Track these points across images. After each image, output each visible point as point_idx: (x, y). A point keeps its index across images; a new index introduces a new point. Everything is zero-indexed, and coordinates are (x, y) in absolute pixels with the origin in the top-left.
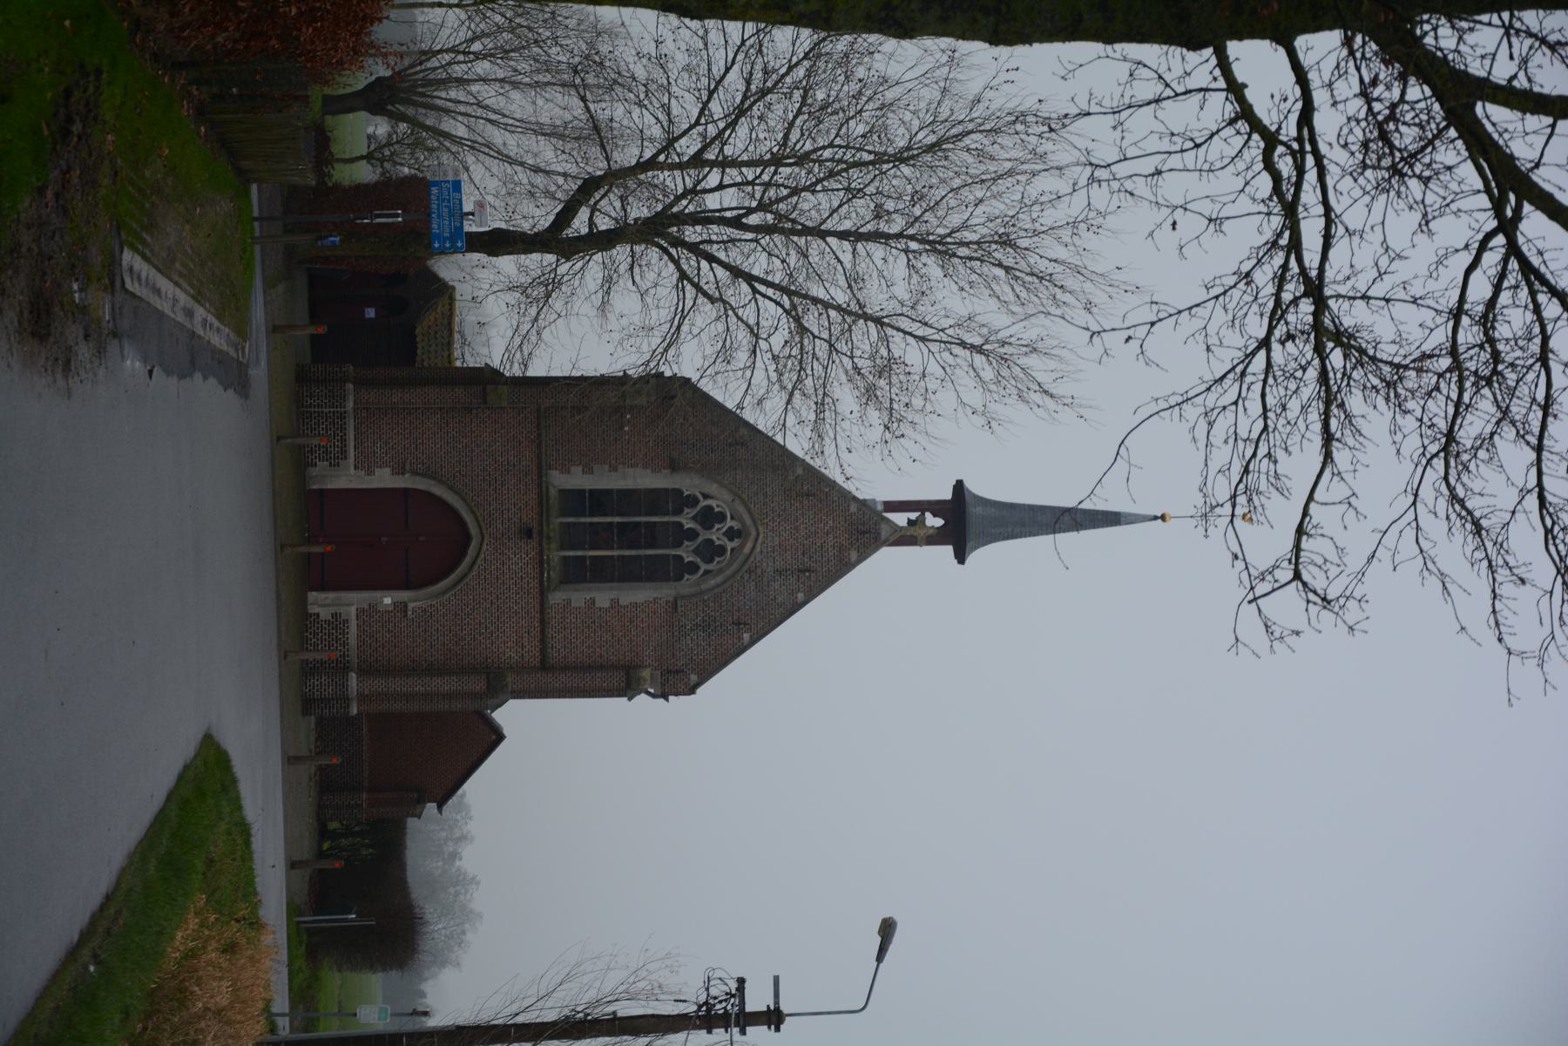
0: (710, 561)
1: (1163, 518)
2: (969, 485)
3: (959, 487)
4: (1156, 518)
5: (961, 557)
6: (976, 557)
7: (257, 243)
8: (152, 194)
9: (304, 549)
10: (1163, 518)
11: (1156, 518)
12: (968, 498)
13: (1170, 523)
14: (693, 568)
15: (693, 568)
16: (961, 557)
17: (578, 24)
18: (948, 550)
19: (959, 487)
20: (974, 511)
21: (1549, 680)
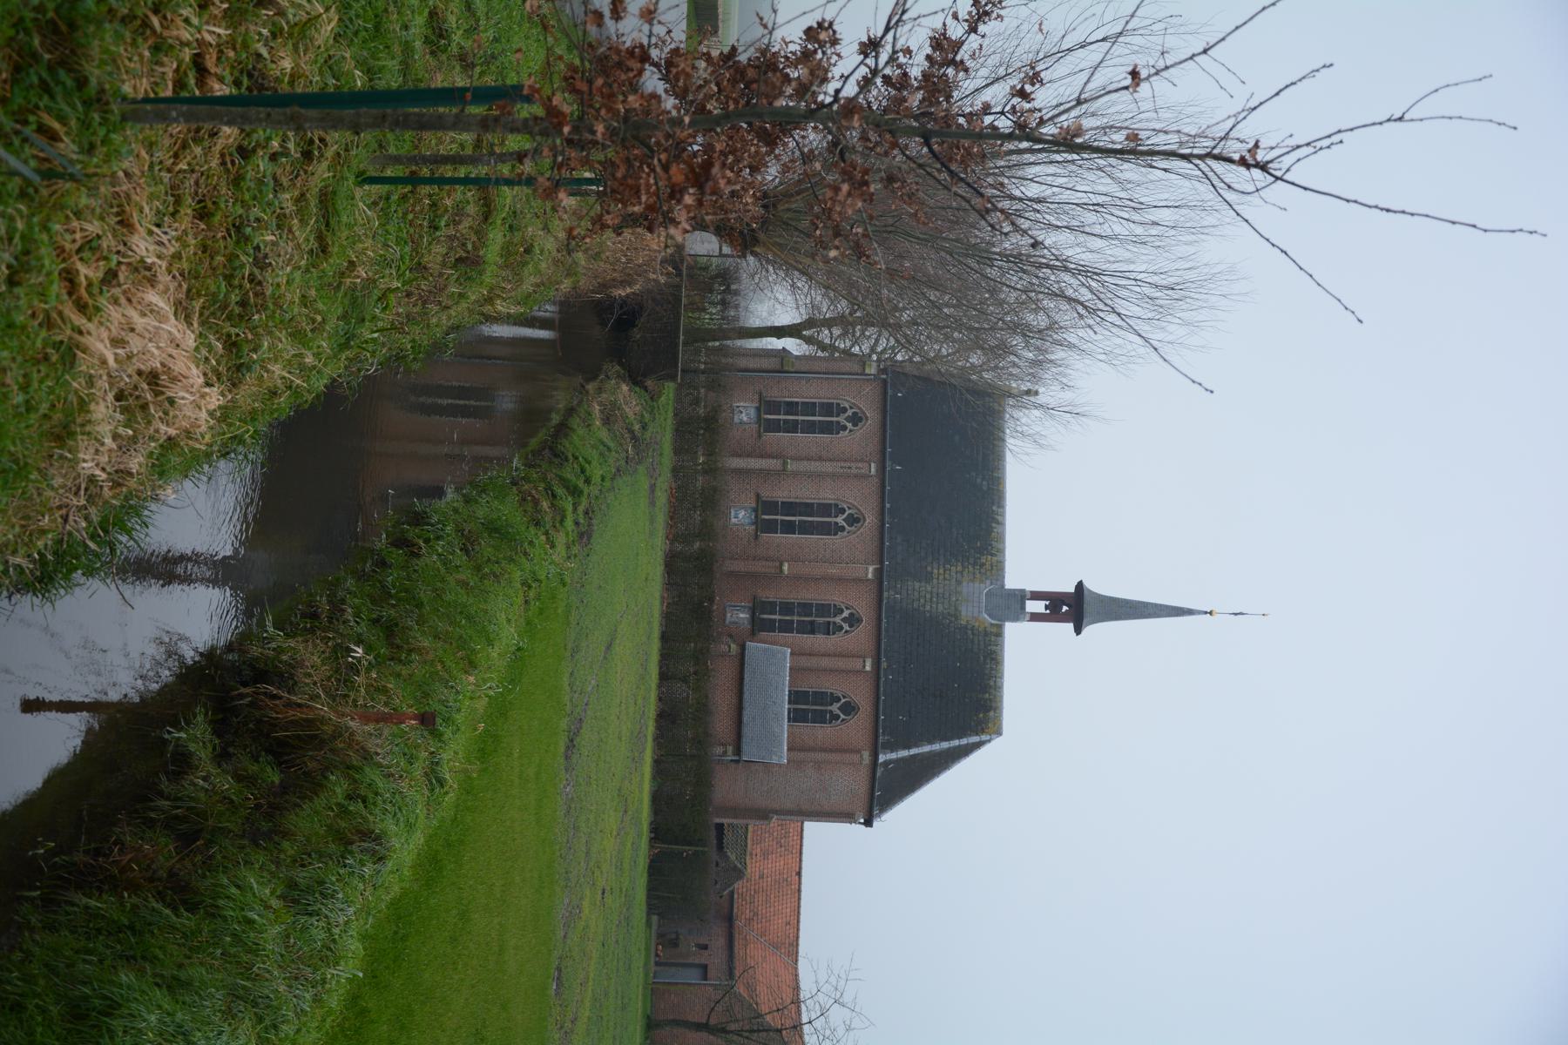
0: (852, 525)
1: (1211, 613)
2: (1087, 584)
3: (1080, 586)
4: (1206, 613)
5: (1078, 631)
6: (1088, 630)
7: (654, 914)
8: (43, 532)
9: (706, 849)
10: (1211, 613)
11: (1206, 613)
12: (1085, 592)
13: (1216, 617)
14: (843, 529)
15: (843, 529)
16: (1078, 631)
17: (538, 217)
18: (1070, 626)
19: (1080, 586)
20: (1087, 598)
21: (1399, 115)
